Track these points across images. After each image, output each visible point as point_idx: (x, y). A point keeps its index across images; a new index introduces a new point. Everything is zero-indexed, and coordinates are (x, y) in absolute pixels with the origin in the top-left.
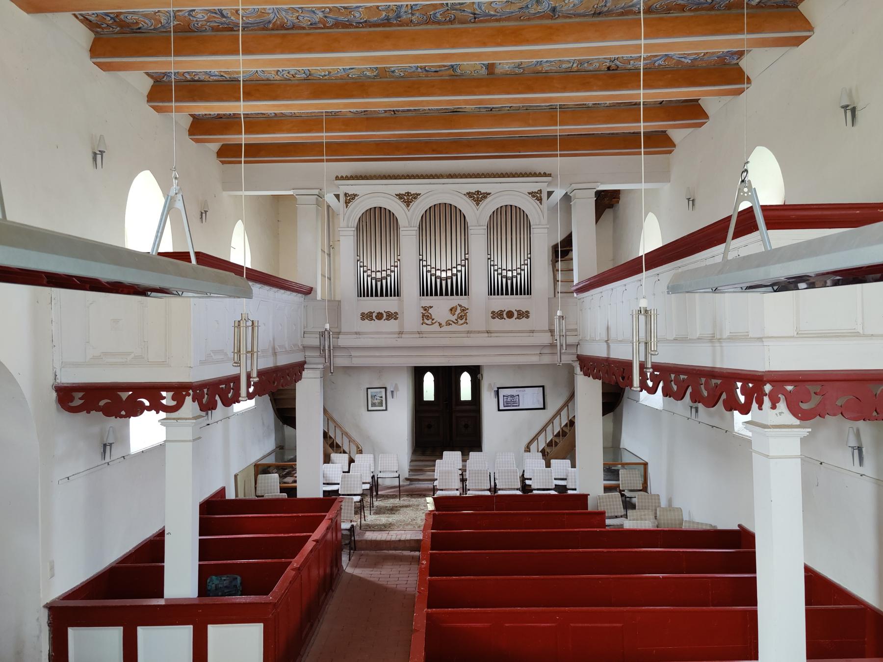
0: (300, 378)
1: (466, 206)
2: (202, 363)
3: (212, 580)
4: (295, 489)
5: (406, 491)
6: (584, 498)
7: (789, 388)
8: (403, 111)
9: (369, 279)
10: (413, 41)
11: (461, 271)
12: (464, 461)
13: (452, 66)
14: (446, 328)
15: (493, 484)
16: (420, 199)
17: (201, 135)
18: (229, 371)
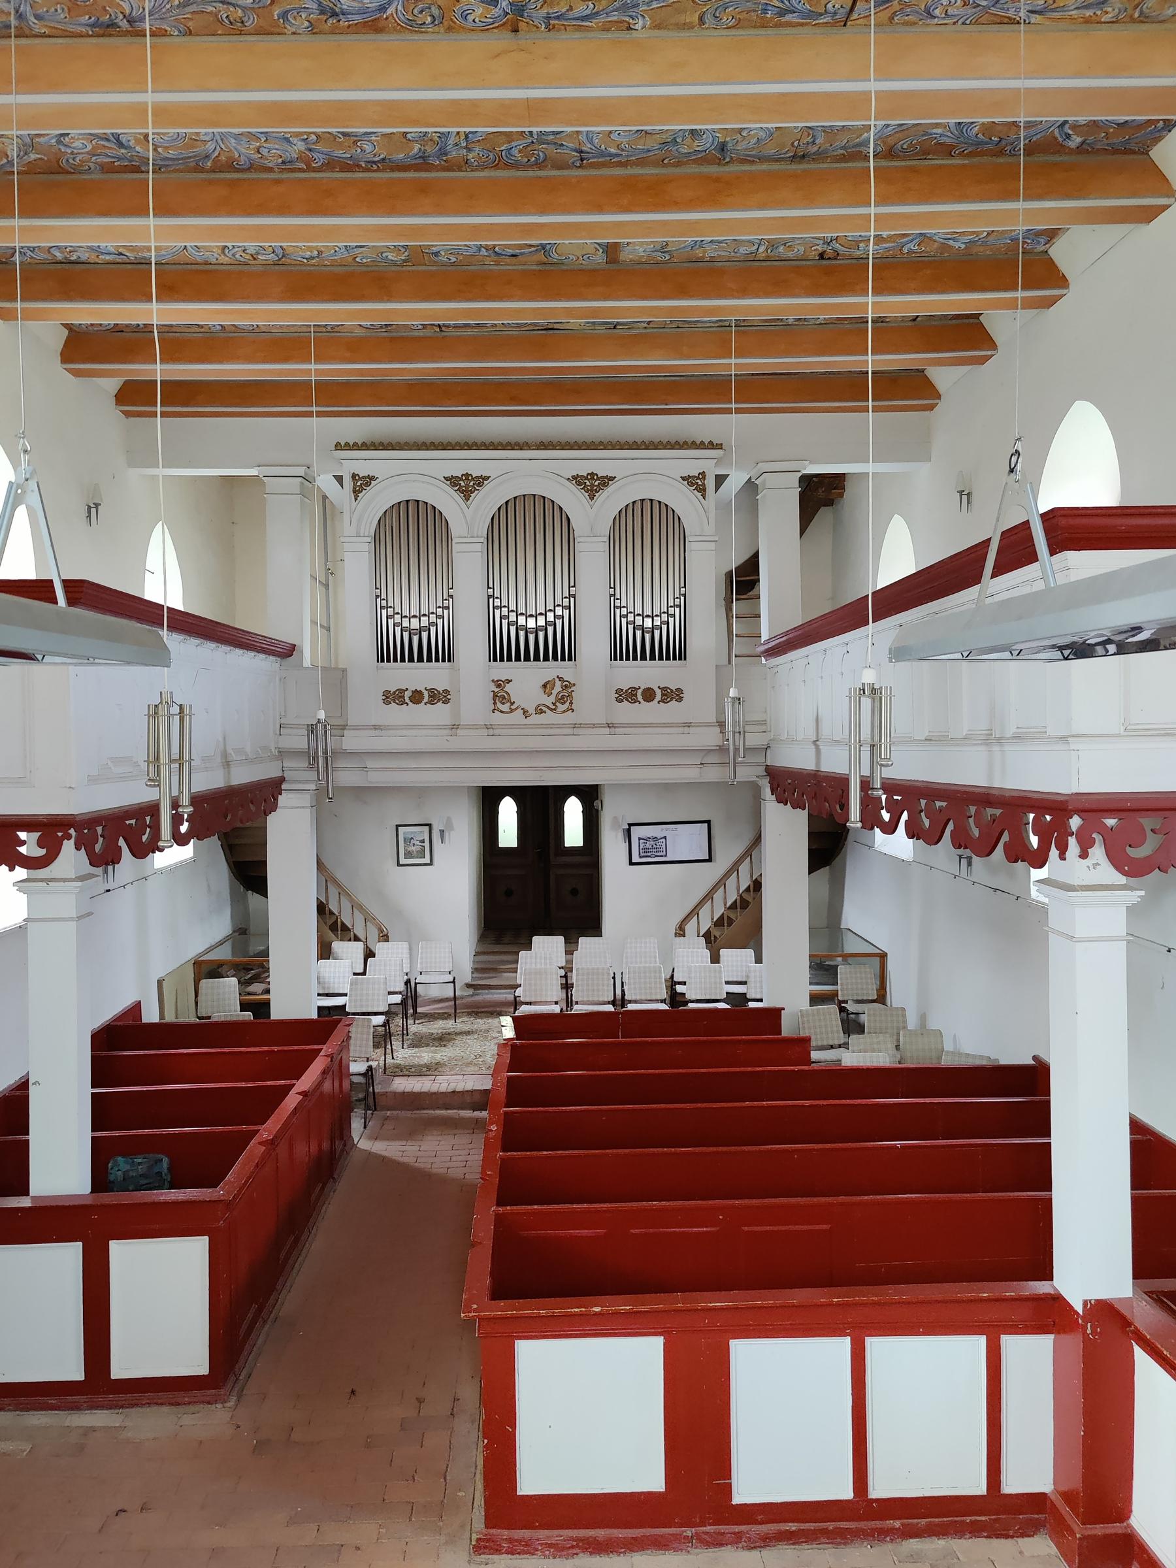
0: (273, 808)
1: (571, 500)
2: (93, 780)
3: (116, 1164)
4: (267, 1004)
5: (467, 1006)
6: (774, 1015)
7: (1111, 822)
8: (456, 327)
9: (398, 630)
10: (470, 201)
11: (674, 616)
12: (569, 953)
13: (543, 247)
14: (535, 719)
15: (619, 992)
16: (488, 487)
17: (84, 362)
18: (140, 794)
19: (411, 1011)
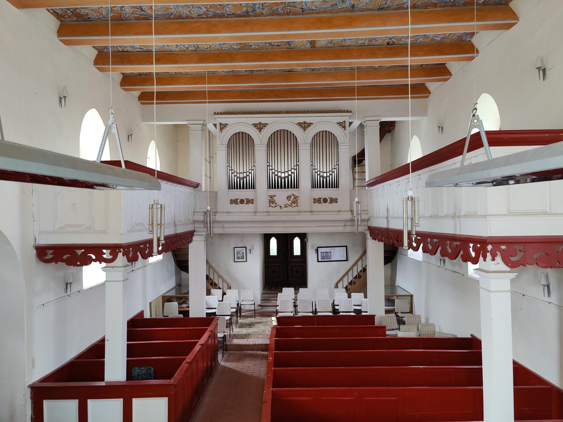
0: (191, 241)
1: (297, 131)
2: (129, 231)
3: (135, 370)
4: (188, 312)
5: (259, 313)
6: (372, 317)
7: (503, 247)
8: (257, 71)
9: (235, 178)
10: (263, 26)
11: (294, 173)
12: (296, 294)
13: (288, 42)
14: (284, 209)
15: (314, 308)
16: (268, 127)
17: (128, 86)
18: (146, 236)
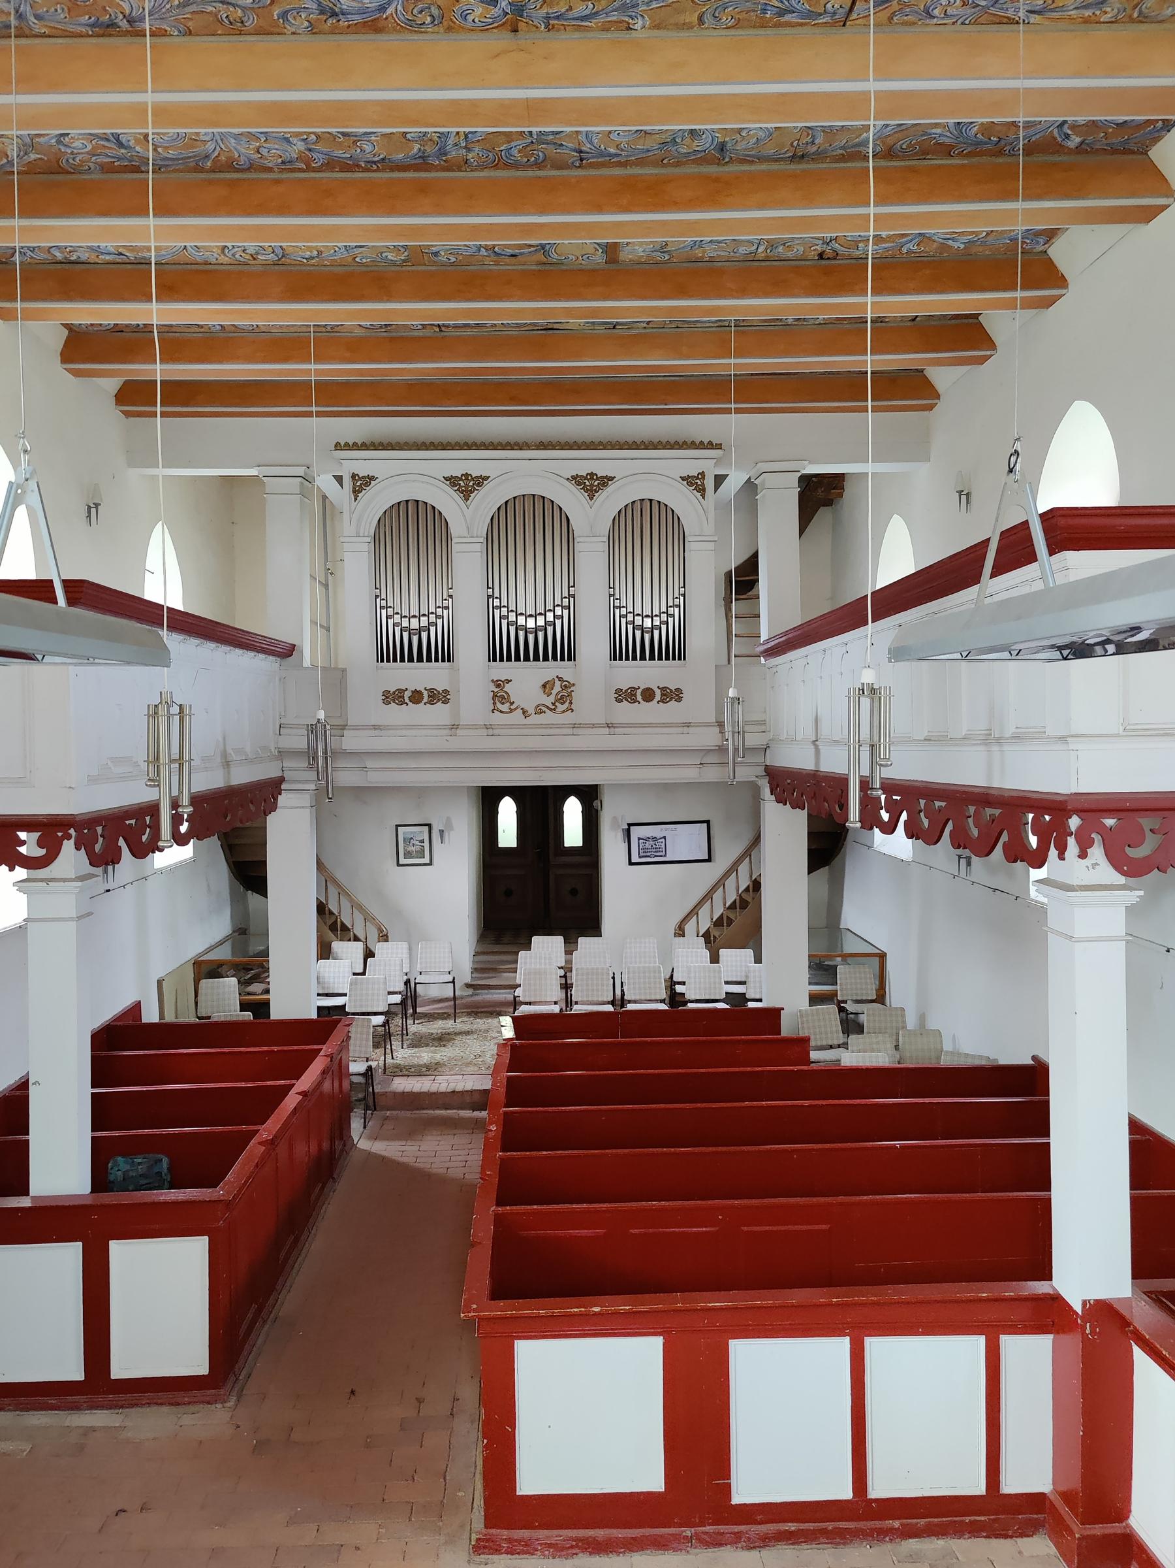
0: (273, 808)
1: (571, 500)
2: (93, 780)
3: (116, 1164)
4: (266, 1004)
5: (467, 1006)
6: (773, 1015)
7: (1110, 822)
8: (456, 327)
9: (398, 630)
10: (469, 201)
11: (673, 616)
12: (569, 953)
13: (543, 247)
14: (535, 719)
15: (618, 992)
16: (487, 487)
17: (84, 362)
18: (140, 794)
19: (410, 1011)
